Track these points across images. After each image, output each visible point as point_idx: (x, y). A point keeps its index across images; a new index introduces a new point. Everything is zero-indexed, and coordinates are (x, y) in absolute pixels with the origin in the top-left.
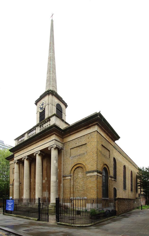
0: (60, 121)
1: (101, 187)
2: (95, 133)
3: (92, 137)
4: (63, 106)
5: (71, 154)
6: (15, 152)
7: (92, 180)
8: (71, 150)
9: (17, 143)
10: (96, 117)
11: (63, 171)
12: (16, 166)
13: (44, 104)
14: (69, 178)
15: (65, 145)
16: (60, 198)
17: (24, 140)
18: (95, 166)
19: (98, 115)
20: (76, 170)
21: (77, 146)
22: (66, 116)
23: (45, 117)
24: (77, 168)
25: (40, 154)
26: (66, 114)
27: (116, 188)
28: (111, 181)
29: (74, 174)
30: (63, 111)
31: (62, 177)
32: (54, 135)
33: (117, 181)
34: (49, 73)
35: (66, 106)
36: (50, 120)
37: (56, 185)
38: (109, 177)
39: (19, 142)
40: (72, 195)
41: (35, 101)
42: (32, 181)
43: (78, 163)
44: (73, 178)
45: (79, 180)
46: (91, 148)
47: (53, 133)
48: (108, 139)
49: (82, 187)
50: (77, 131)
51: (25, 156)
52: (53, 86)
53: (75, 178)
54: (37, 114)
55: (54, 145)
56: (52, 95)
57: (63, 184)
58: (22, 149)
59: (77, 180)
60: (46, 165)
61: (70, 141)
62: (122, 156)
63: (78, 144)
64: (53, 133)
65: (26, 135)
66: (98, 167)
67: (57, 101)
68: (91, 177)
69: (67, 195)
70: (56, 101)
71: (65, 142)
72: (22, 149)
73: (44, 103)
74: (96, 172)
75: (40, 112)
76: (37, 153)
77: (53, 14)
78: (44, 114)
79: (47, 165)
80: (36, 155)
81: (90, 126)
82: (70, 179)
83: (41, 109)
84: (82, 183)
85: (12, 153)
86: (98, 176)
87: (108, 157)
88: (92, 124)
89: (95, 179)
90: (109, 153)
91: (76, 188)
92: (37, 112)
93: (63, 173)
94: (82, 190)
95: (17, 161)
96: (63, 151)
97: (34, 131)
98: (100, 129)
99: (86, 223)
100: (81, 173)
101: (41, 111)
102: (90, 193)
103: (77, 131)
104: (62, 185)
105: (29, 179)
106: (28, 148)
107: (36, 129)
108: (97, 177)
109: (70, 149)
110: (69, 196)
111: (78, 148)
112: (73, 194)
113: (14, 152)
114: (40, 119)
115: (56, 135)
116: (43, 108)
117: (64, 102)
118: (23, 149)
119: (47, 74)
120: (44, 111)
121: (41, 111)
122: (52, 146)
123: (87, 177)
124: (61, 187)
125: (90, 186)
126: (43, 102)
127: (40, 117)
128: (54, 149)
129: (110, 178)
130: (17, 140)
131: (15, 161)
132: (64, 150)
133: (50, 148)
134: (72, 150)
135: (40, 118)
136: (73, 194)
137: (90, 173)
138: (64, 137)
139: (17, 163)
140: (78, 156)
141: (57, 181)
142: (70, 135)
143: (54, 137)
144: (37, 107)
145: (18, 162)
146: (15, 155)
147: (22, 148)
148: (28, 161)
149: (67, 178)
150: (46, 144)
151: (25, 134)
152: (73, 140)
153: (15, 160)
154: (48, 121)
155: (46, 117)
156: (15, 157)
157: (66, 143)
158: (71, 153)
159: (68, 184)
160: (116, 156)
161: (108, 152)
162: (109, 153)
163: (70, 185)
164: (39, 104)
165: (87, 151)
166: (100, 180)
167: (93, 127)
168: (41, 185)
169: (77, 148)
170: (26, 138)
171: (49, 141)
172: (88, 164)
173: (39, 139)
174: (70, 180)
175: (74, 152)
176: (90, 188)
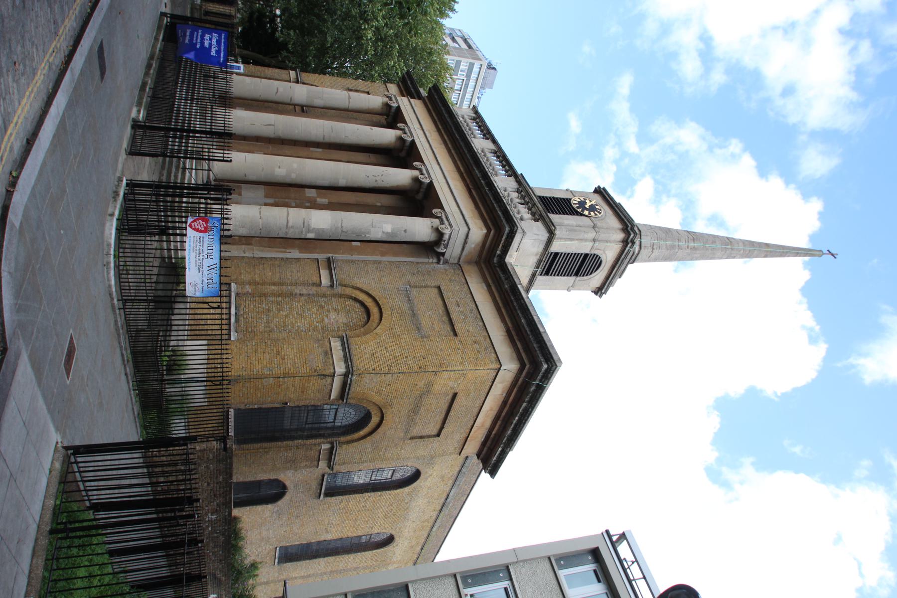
0: (536, 255)
1: (281, 398)
2: (495, 362)
3: (479, 352)
4: (598, 278)
5: (422, 287)
6: (430, 102)
7: (312, 357)
8: (435, 287)
9: (463, 114)
10: (542, 359)
11: (352, 261)
12: (375, 101)
13: (596, 214)
14: (325, 281)
15: (454, 269)
16: (230, 141)
17: (475, 138)
18: (371, 365)
19: (548, 364)
20: (357, 305)
21: (449, 307)
22: (568, 290)
23: (553, 213)
24: (362, 309)
25: (421, 183)
26: (574, 292)
27: (286, 498)
28: (313, 453)
29: (341, 296)
30: (582, 278)
31: (330, 255)
32: (485, 231)
33: (316, 501)
34: (690, 236)
35: (600, 291)
36: (536, 220)
37: (292, 227)
38: (332, 443)
39: (465, 122)
40: (248, 289)
41: (604, 189)
42: (312, 151)
43: (383, 311)
44: (324, 296)
45: (316, 314)
46: (441, 350)
47: (491, 227)
48: (483, 425)
49: (285, 326)
50: (403, 89)
51: (411, 133)
52: (655, 247)
53: (325, 302)
54: (567, 190)
55: (449, 227)
56: (623, 242)
57: (298, 260)
58: (440, 127)
59: (314, 310)
60: (379, 204)
61: (466, 285)
62: (434, 518)
63: (457, 309)
64: (491, 227)
65: (488, 145)
66: (367, 379)
67: (609, 255)
68: (326, 353)
69: (249, 270)
70: (606, 252)
71: (466, 268)
72: (440, 127)
73: (600, 213)
74: (347, 367)
75: (570, 199)
76: (424, 171)
77: (835, 258)
78: (564, 213)
79: (379, 206)
80: (417, 169)
81: (516, 345)
82: (318, 282)
83: (582, 204)
84: (302, 324)
85: (424, 93)
86: (329, 380)
87: (415, 431)
88: (521, 351)
89: (320, 366)
90: (429, 437)
91: (278, 303)
92: (571, 192)
93: (346, 261)
94: (272, 325)
95: (410, 139)
96: (431, 260)
97: (504, 172)
98: (509, 386)
99: (122, 284)
100: (344, 320)
101: (574, 202)
102: (256, 351)
103: (501, 305)
104: (295, 254)
105: (320, 139)
106: (443, 146)
107: (535, 220)
108: (325, 376)
109: (437, 284)
110: (245, 277)
111: (441, 310)
112: (253, 295)
113: (429, 100)
114: (550, 198)
115: (487, 236)
116: (583, 211)
117: (611, 284)
118: (439, 130)
119: (688, 231)
120: (573, 212)
121: (574, 204)
122: (448, 220)
123: (327, 340)
124: (283, 250)
125: (290, 352)
126: (602, 214)
127: (557, 198)
128: (435, 226)
129: (325, 446)
130: (474, 115)
131: (397, 100)
132: (435, 265)
133: (439, 215)
134: (436, 291)
135: (553, 198)
136: (253, 295)
137: (341, 352)
138: (483, 266)
139: (387, 106)
140: (412, 309)
141: (309, 231)
142: (489, 286)
143: (478, 232)
144: (587, 193)
145: (420, 187)
146: (417, 103)
147: (444, 129)
148: (395, 142)
149: (324, 274)
150: (454, 203)
151: (494, 141)
152: (470, 296)
153: (398, 98)
154: (533, 214)
155: (555, 218)
156: (412, 100)
157: (461, 274)
158: (425, 287)
159: (299, 274)
160: (428, 483)
161: (435, 432)
162: (429, 437)
163: (291, 284)
164: (597, 200)
165: (427, 338)
166: (312, 394)
167: (514, 355)
168: (293, 176)
169: (443, 308)
170: (479, 143)
171: (450, 183)
172: (378, 344)
173: (471, 182)
174: (314, 284)
175: (426, 301)
176: (278, 353)
